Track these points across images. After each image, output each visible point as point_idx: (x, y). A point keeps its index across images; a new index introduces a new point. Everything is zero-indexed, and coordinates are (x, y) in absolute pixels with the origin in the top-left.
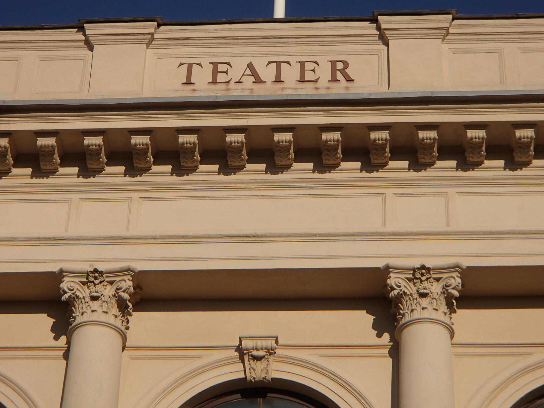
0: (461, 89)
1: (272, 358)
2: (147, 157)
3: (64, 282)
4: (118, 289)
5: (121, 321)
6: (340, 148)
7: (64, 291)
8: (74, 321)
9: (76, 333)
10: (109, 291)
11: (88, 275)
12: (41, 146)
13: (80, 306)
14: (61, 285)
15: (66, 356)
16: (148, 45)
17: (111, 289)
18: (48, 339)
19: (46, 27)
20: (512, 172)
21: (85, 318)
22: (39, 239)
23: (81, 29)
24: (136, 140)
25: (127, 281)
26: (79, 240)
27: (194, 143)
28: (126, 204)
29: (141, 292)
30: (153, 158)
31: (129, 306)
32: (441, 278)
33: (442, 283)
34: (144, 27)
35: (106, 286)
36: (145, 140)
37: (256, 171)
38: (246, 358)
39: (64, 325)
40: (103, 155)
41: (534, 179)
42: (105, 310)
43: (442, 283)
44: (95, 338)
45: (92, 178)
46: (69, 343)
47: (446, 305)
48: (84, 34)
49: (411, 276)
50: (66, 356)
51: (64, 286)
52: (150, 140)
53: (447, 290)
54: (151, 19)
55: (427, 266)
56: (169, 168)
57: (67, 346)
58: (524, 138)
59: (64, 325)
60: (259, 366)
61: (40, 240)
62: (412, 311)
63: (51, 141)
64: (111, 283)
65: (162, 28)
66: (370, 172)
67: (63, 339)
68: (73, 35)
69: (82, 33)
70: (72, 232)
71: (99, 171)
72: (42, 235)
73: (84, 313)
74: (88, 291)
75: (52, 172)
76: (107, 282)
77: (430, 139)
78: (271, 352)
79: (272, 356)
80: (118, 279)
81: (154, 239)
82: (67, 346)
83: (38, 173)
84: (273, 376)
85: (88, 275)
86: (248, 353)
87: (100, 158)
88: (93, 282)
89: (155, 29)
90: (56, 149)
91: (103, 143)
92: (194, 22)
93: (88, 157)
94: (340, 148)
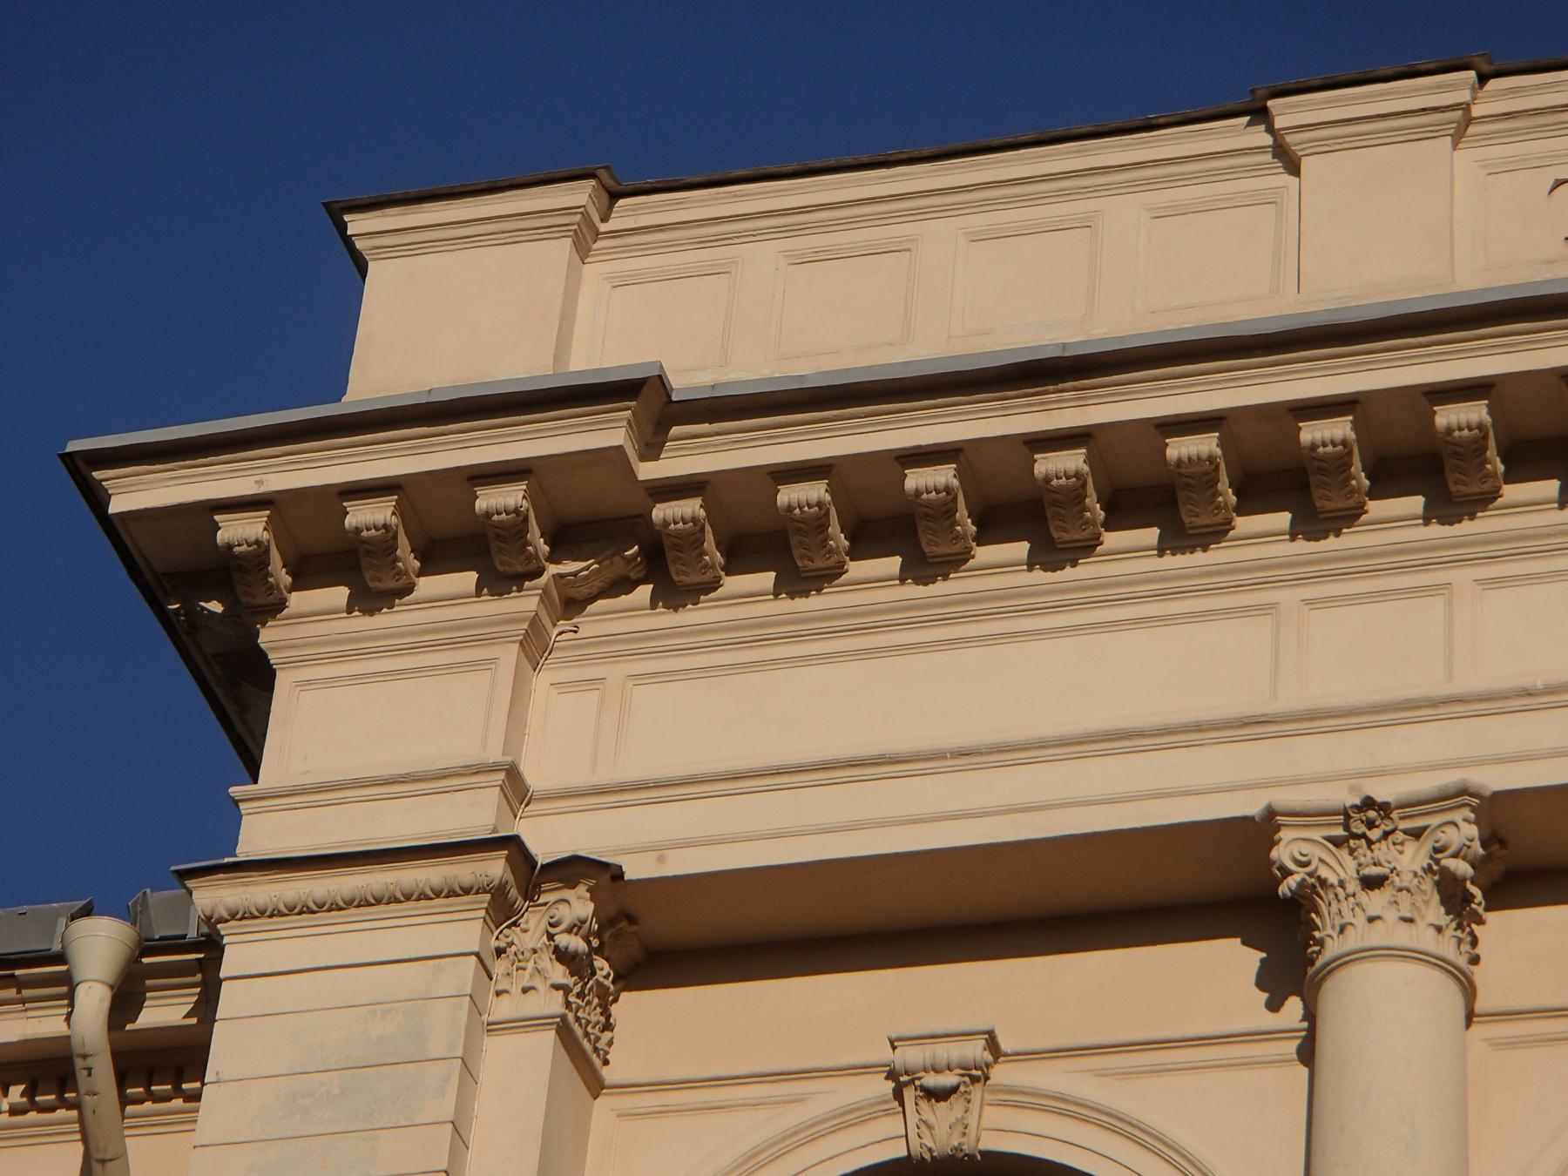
0: (925, 354)
1: (976, 1091)
2: (1217, 494)
3: (1282, 844)
4: (1437, 850)
5: (1454, 941)
6: (1492, 443)
7: (1282, 868)
8: (1319, 952)
9: (1328, 985)
10: (1413, 859)
11: (1348, 817)
12: (1179, 461)
13: (1334, 908)
14: (1274, 854)
15: (1307, 1053)
16: (1458, 138)
17: (1418, 850)
18: (1250, 1008)
19: (1161, 121)
20: (1447, 527)
21: (1352, 941)
22: (1198, 727)
23: (1260, 115)
24: (1448, 416)
25: (1463, 825)
26: (1312, 719)
27: (1480, 426)
28: (1436, 605)
29: (1504, 852)
30: (1503, 462)
31: (1473, 896)
32: (1425, 828)
33: (1427, 844)
34: (1440, 88)
35: (1402, 844)
36: (1475, 412)
37: (1130, 550)
38: (909, 1095)
39: (1293, 965)
40: (1357, 468)
41: (1548, 536)
42: (1407, 914)
43: (1427, 844)
44: (1386, 993)
45: (1068, 570)
46: (1310, 1016)
47: (1443, 903)
48: (1271, 130)
49: (1340, 832)
50: (1307, 1053)
51: (1282, 853)
52: (1490, 413)
53: (1437, 862)
54: (1457, 62)
55: (1379, 799)
56: (1416, 503)
57: (1305, 1024)
58: (1058, 478)
59: (1293, 965)
60: (943, 1115)
61: (1201, 731)
62: (1342, 930)
63: (1205, 445)
64: (1417, 834)
65: (1493, 84)
66: (675, 607)
67: (1294, 1007)
68: (1238, 134)
69: (1263, 127)
70: (1291, 700)
71: (1351, 517)
72: (1206, 716)
73: (1346, 926)
74: (1350, 863)
75: (1217, 533)
76: (1405, 832)
77: (1334, 445)
78: (977, 1075)
79: (978, 1086)
80: (1434, 821)
81: (1526, 698)
82: (1305, 1024)
83: (1178, 539)
84: (983, 1146)
85: (1348, 817)
86: (913, 1081)
87: (1351, 477)
88: (1364, 836)
89: (1473, 89)
90: (1491, 433)
91: (1353, 436)
92: (983, 142)
93: (1314, 479)
94: (1492, 443)
